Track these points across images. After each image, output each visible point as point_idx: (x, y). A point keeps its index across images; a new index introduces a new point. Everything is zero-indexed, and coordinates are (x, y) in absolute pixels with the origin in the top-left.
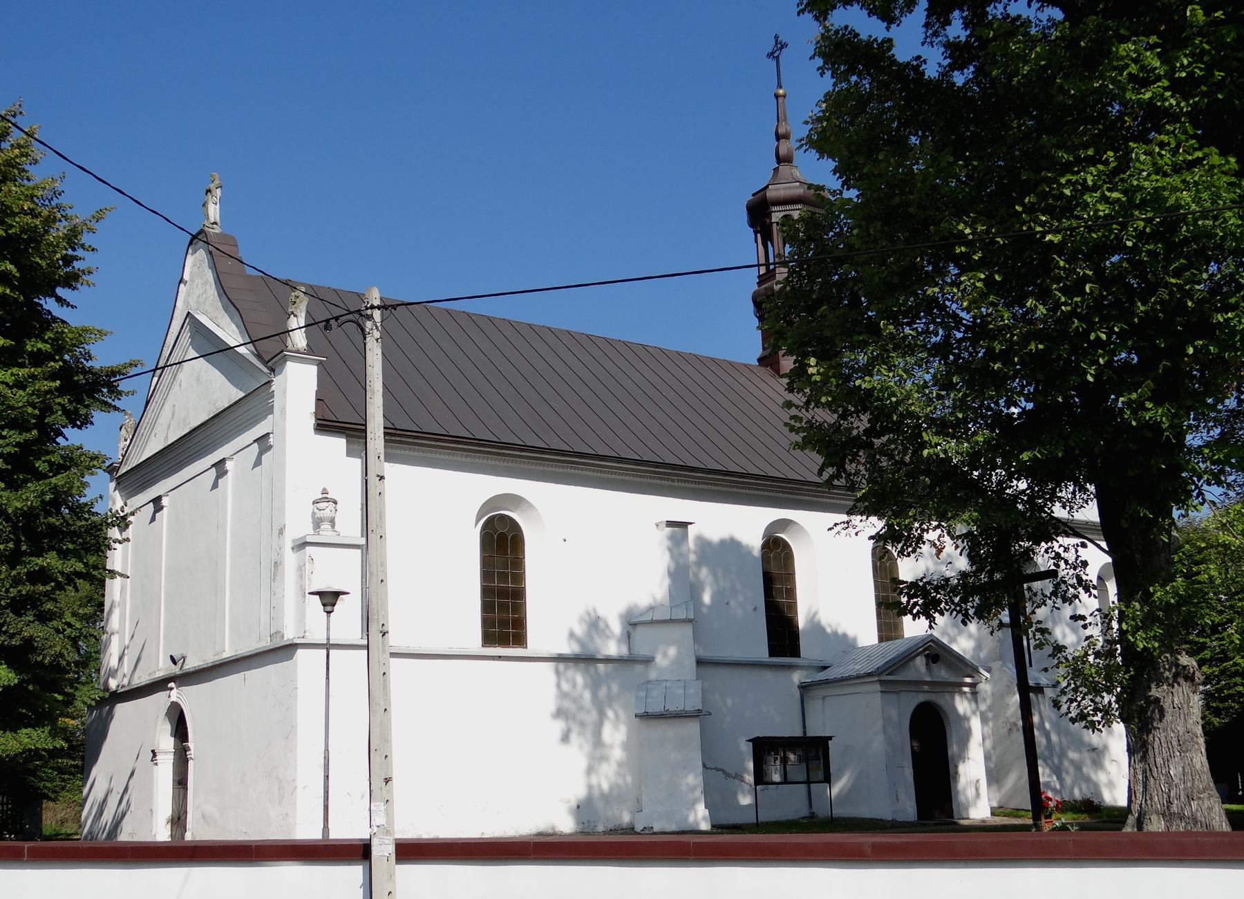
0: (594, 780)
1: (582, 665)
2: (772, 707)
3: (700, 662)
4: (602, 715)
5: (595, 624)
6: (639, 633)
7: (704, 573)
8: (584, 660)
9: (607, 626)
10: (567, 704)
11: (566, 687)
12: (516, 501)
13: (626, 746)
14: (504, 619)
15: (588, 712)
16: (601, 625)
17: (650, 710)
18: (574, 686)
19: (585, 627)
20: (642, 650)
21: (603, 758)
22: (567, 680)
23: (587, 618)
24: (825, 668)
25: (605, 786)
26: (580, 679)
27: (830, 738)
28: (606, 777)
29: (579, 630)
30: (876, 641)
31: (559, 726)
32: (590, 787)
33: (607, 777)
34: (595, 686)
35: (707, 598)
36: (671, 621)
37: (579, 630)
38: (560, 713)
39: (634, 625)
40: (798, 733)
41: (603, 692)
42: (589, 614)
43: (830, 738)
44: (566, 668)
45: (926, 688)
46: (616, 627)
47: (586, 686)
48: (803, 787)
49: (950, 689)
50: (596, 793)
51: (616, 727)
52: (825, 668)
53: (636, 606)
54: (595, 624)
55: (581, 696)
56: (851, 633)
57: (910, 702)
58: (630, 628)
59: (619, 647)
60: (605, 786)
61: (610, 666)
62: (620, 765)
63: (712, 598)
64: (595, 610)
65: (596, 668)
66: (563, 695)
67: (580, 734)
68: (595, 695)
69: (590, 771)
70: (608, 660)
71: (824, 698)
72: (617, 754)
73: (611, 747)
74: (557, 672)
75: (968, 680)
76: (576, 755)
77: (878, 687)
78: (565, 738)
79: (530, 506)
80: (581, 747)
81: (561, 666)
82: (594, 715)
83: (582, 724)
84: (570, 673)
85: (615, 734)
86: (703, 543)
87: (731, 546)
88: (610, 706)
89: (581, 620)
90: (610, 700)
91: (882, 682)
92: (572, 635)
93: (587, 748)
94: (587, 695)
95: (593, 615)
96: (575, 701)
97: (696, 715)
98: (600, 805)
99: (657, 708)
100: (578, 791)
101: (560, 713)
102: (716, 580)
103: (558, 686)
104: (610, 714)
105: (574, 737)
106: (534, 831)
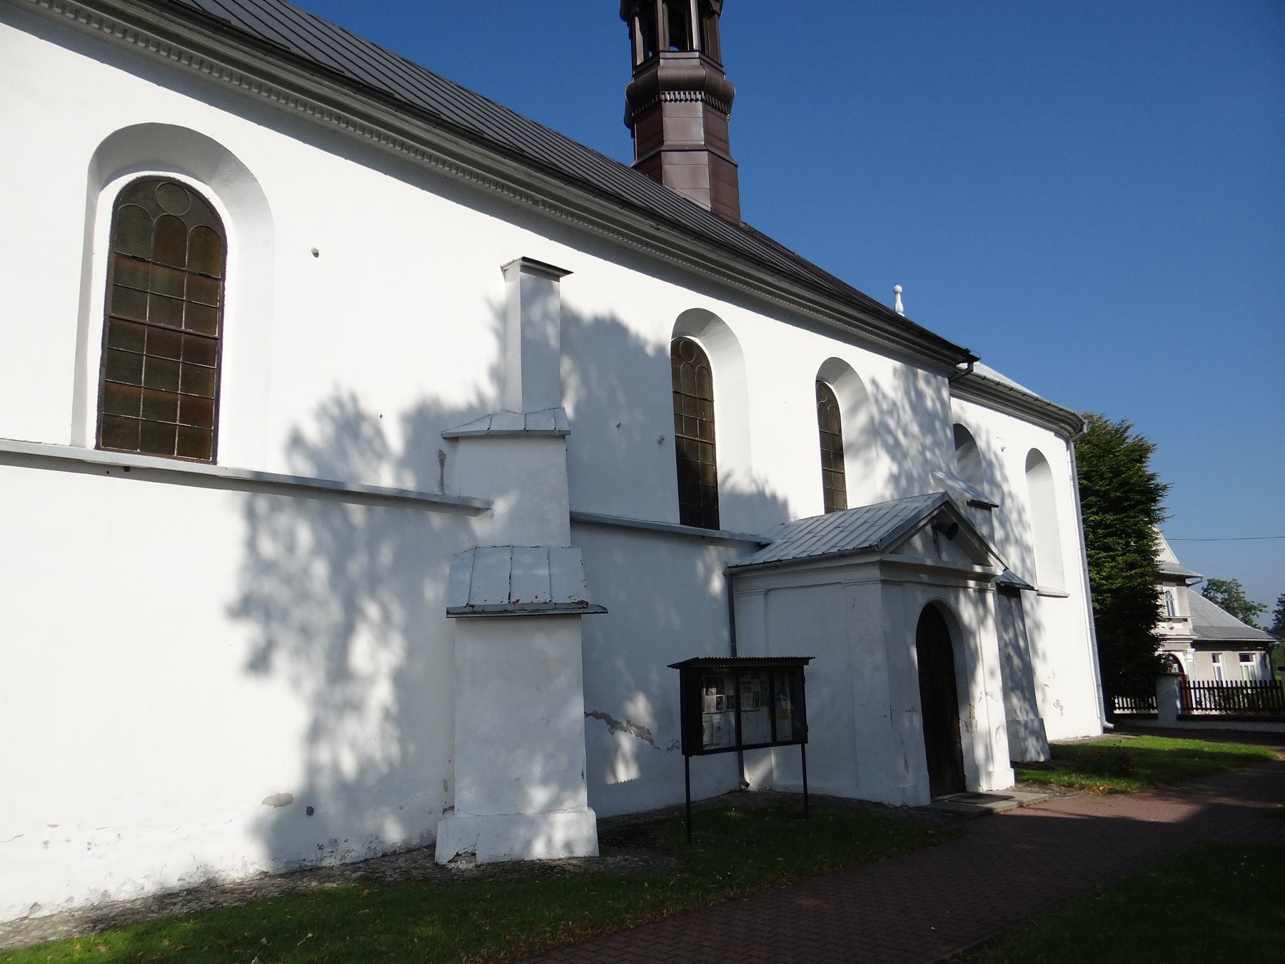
0: (324, 754)
1: (313, 503)
2: (688, 600)
3: (578, 521)
4: (352, 613)
5: (350, 424)
6: (463, 456)
7: (566, 365)
8: (317, 492)
9: (379, 433)
10: (269, 586)
11: (268, 548)
12: (212, 155)
13: (400, 679)
14: (158, 385)
15: (322, 604)
16: (367, 430)
17: (478, 601)
18: (291, 547)
19: (329, 429)
20: (460, 487)
21: (354, 706)
22: (274, 535)
23: (335, 411)
24: (760, 546)
25: (349, 764)
26: (305, 535)
27: (806, 661)
28: (364, 739)
29: (314, 432)
30: (823, 512)
31: (243, 636)
32: (312, 770)
33: (353, 745)
34: (339, 551)
35: (569, 408)
36: (525, 435)
37: (314, 432)
38: (246, 607)
39: (454, 439)
40: (724, 653)
41: (356, 566)
42: (340, 404)
43: (806, 661)
44: (276, 508)
45: (925, 577)
46: (395, 438)
47: (318, 549)
48: (733, 744)
49: (952, 582)
50: (325, 782)
51: (382, 640)
52: (760, 546)
53: (437, 402)
54: (350, 424)
55: (305, 571)
56: (780, 494)
57: (919, 598)
58: (445, 446)
59: (398, 476)
60: (349, 764)
61: (380, 510)
62: (387, 715)
63: (577, 409)
64: (354, 398)
65: (345, 516)
66: (258, 565)
67: (297, 652)
68: (338, 570)
69: (315, 733)
70: (372, 498)
71: (767, 592)
72: (381, 694)
73: (371, 680)
74: (251, 515)
75: (978, 569)
76: (283, 704)
77: (876, 573)
78: (259, 663)
79: (240, 170)
80: (296, 683)
81: (262, 503)
82: (335, 612)
83: (305, 632)
84: (284, 520)
85: (375, 656)
86: (569, 320)
87: (610, 332)
88: (373, 594)
89: (321, 413)
90: (373, 582)
91: (883, 565)
92: (296, 441)
93: (313, 682)
94: (320, 569)
95: (349, 407)
96: (288, 580)
97: (574, 612)
98: (329, 807)
99: (493, 597)
100: (286, 776)
101: (246, 607)
102: (585, 380)
103: (251, 544)
104: (373, 611)
105: (281, 660)
106: (150, 888)
